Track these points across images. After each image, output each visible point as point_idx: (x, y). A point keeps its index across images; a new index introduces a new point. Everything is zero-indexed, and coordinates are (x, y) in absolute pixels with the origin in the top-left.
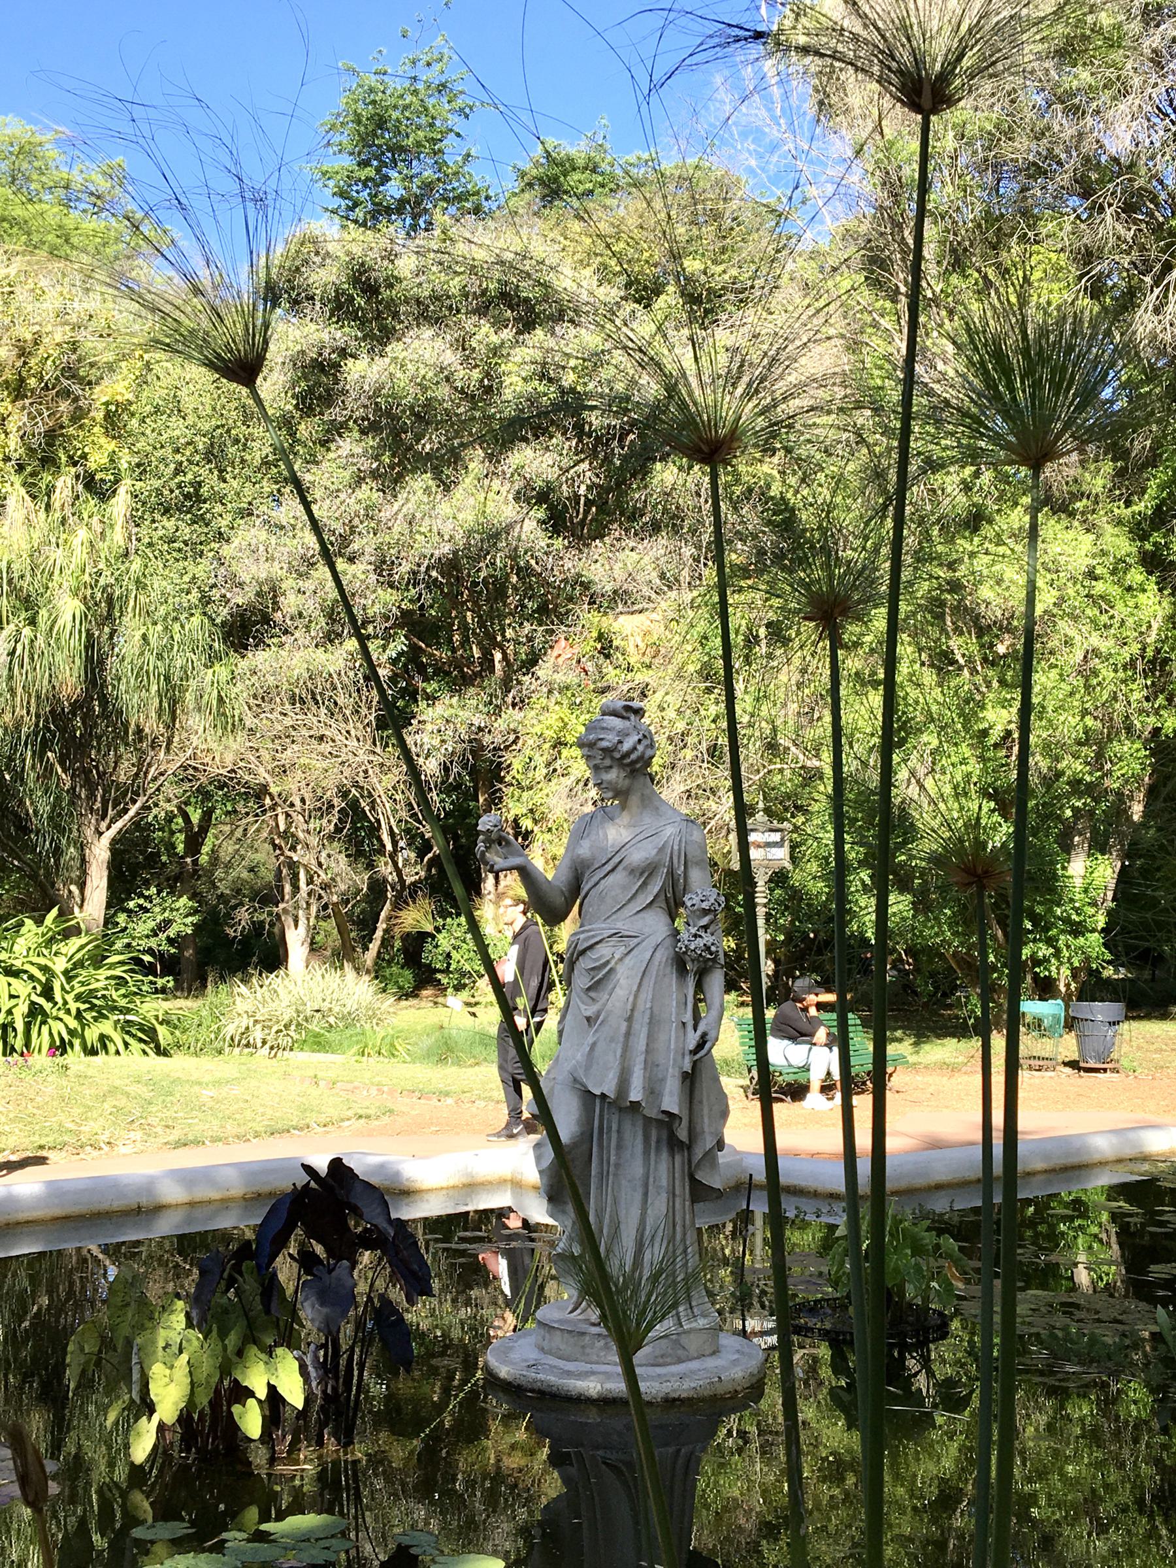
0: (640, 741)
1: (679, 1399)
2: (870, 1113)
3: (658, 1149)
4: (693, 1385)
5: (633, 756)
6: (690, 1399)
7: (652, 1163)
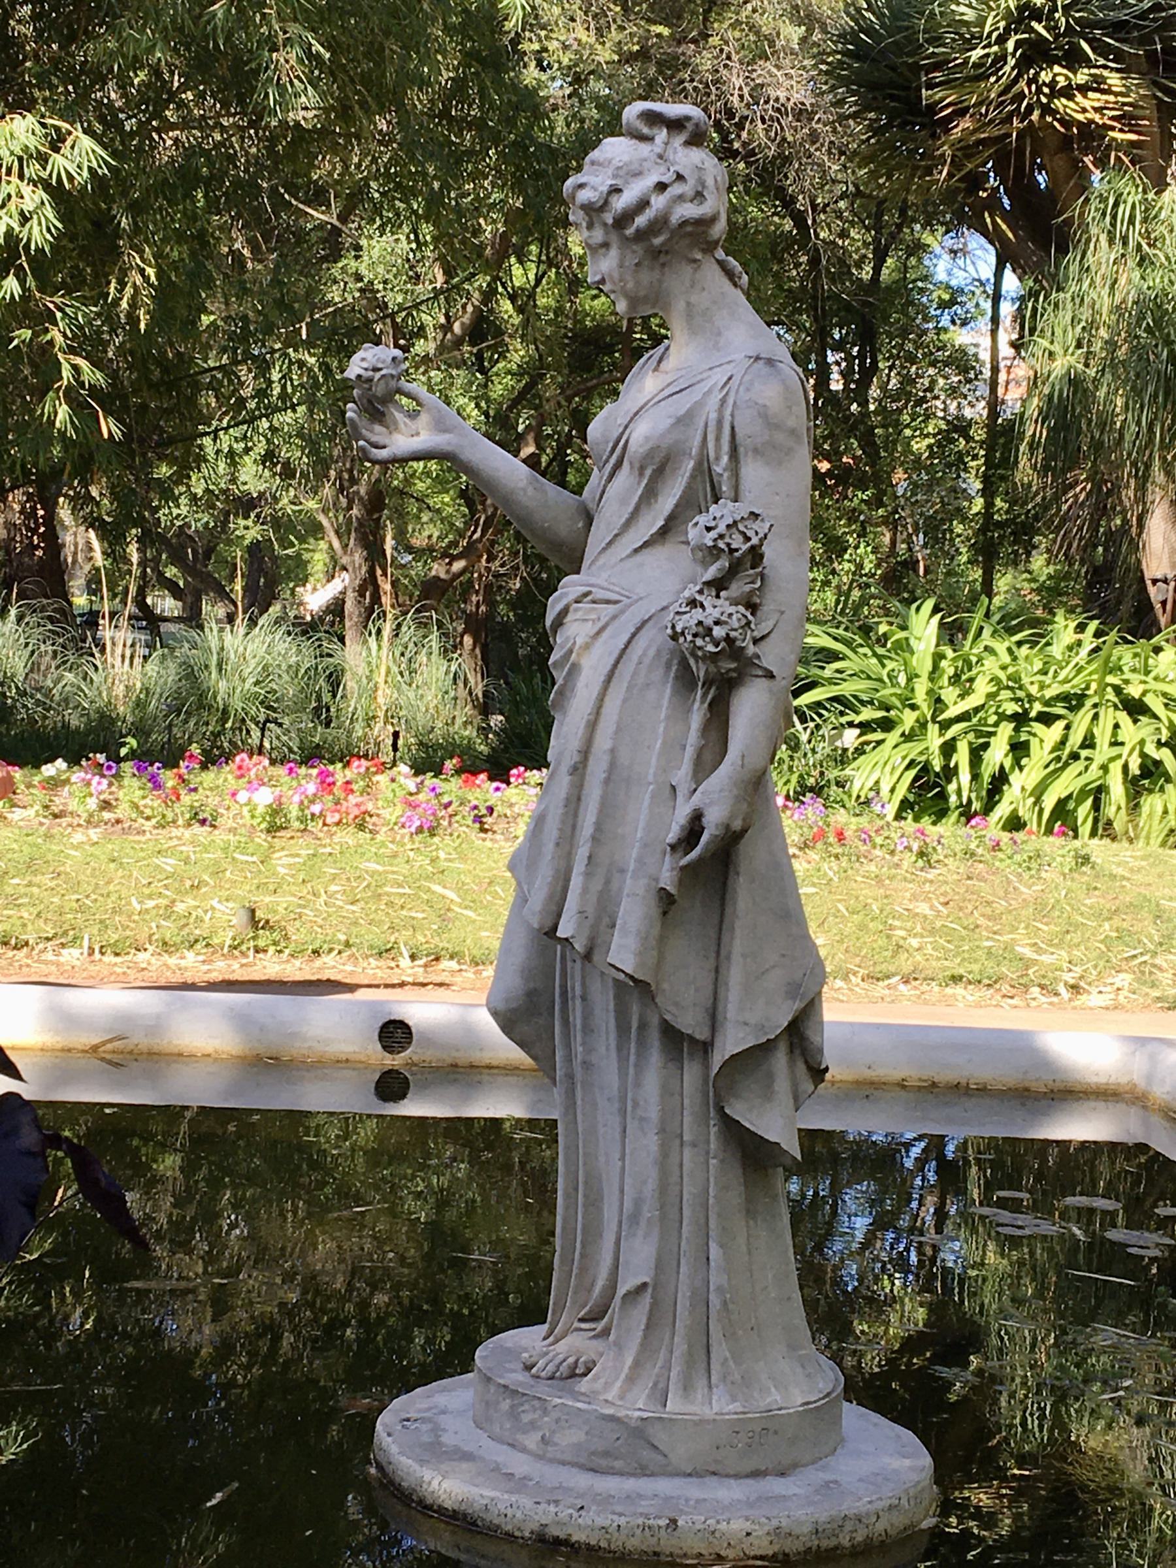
0: (661, 187)
1: (566, 1542)
2: (299, 976)
3: (642, 1043)
4: (600, 1521)
5: (641, 221)
6: (592, 1550)
7: (631, 1071)
